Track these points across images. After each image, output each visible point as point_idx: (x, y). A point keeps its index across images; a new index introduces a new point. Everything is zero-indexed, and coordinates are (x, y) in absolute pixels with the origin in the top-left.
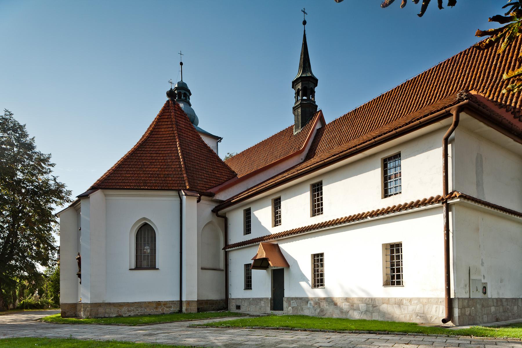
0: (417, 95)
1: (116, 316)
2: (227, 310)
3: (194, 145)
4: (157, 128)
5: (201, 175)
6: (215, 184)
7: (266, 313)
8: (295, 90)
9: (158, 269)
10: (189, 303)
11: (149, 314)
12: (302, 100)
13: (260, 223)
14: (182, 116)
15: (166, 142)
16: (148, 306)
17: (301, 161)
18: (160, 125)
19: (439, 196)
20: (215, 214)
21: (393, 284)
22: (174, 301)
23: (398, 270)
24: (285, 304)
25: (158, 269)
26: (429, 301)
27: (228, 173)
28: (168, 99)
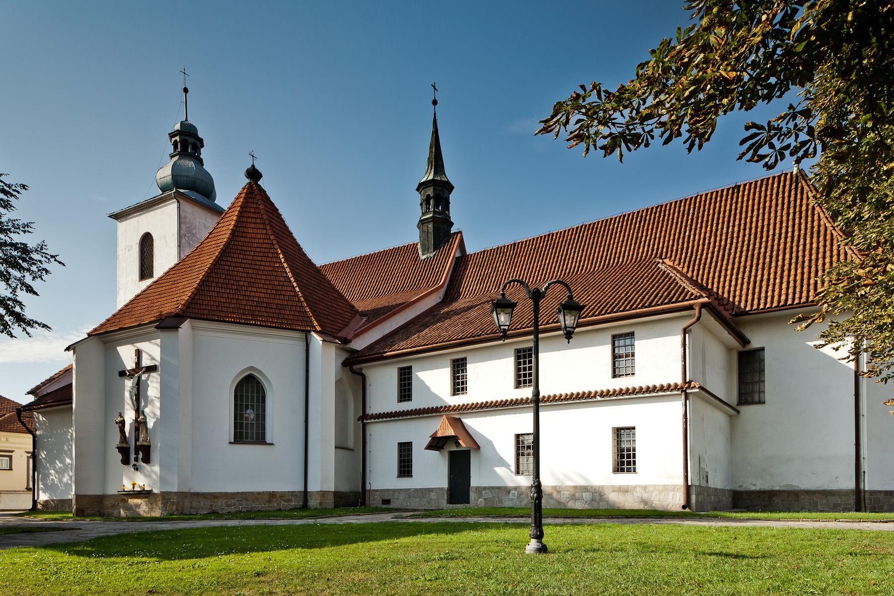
0: (600, 247)
1: (208, 513)
4: (240, 227)
10: (323, 494)
11: (259, 510)
13: (429, 388)
16: (257, 499)
21: (622, 470)
24: (472, 496)
26: (665, 488)
28: (248, 181)
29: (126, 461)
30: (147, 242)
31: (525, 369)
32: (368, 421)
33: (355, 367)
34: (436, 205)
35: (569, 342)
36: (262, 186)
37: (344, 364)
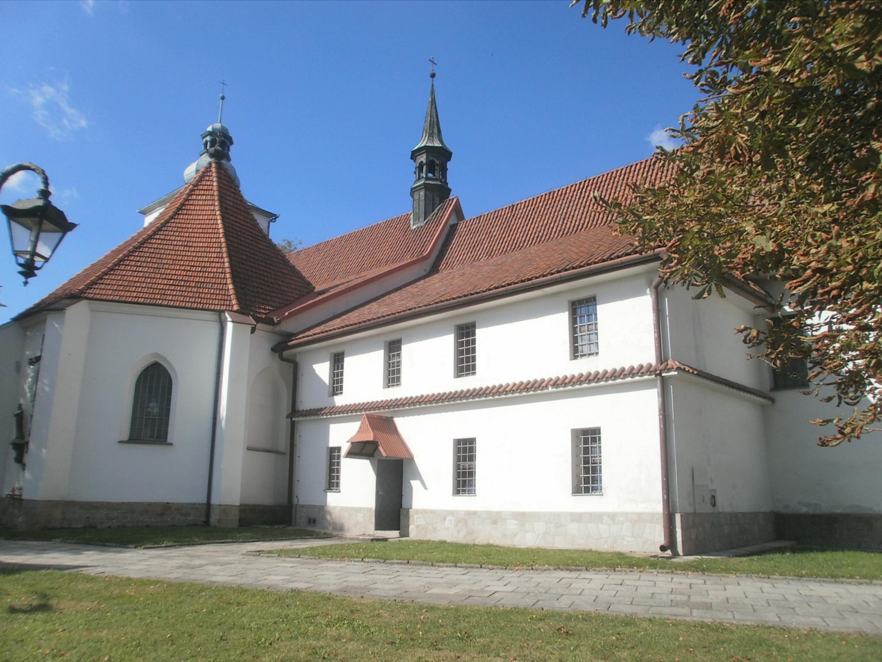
2: (290, 525)
3: (246, 236)
5: (256, 287)
6: (280, 303)
7: (367, 533)
8: (415, 161)
9: (171, 444)
10: (225, 509)
12: (427, 178)
14: (231, 187)
15: (200, 228)
17: (424, 273)
18: (194, 200)
19: (650, 365)
20: (277, 354)
21: (587, 490)
22: (195, 504)
23: (594, 470)
25: (171, 444)
27: (301, 285)
32: (301, 419)
35: (26, 283)
37: (274, 350)
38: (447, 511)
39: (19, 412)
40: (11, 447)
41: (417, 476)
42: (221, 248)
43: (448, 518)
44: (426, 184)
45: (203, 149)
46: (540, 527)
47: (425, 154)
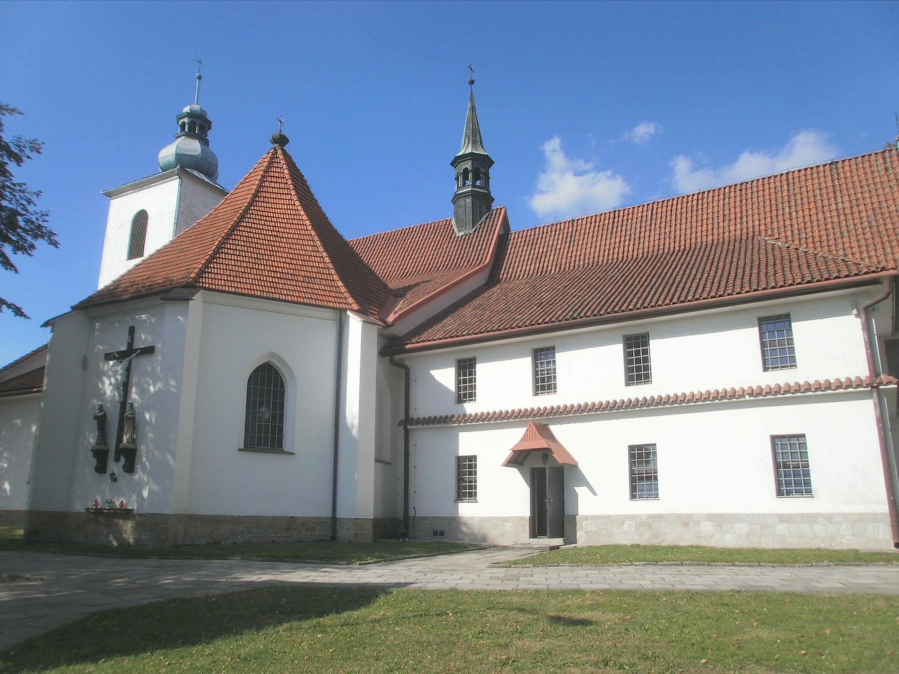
11: (273, 541)
29: (101, 469)
30: (140, 222)
31: (638, 361)
32: (414, 427)
33: (397, 357)
34: (476, 178)
36: (288, 151)
38: (625, 516)
39: (102, 414)
40: (91, 453)
41: (583, 482)
42: (314, 241)
43: (626, 523)
44: (474, 191)
45: (179, 132)
46: (742, 528)
47: (471, 161)
